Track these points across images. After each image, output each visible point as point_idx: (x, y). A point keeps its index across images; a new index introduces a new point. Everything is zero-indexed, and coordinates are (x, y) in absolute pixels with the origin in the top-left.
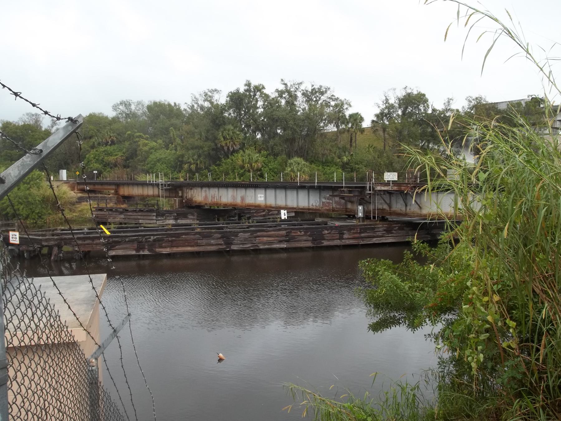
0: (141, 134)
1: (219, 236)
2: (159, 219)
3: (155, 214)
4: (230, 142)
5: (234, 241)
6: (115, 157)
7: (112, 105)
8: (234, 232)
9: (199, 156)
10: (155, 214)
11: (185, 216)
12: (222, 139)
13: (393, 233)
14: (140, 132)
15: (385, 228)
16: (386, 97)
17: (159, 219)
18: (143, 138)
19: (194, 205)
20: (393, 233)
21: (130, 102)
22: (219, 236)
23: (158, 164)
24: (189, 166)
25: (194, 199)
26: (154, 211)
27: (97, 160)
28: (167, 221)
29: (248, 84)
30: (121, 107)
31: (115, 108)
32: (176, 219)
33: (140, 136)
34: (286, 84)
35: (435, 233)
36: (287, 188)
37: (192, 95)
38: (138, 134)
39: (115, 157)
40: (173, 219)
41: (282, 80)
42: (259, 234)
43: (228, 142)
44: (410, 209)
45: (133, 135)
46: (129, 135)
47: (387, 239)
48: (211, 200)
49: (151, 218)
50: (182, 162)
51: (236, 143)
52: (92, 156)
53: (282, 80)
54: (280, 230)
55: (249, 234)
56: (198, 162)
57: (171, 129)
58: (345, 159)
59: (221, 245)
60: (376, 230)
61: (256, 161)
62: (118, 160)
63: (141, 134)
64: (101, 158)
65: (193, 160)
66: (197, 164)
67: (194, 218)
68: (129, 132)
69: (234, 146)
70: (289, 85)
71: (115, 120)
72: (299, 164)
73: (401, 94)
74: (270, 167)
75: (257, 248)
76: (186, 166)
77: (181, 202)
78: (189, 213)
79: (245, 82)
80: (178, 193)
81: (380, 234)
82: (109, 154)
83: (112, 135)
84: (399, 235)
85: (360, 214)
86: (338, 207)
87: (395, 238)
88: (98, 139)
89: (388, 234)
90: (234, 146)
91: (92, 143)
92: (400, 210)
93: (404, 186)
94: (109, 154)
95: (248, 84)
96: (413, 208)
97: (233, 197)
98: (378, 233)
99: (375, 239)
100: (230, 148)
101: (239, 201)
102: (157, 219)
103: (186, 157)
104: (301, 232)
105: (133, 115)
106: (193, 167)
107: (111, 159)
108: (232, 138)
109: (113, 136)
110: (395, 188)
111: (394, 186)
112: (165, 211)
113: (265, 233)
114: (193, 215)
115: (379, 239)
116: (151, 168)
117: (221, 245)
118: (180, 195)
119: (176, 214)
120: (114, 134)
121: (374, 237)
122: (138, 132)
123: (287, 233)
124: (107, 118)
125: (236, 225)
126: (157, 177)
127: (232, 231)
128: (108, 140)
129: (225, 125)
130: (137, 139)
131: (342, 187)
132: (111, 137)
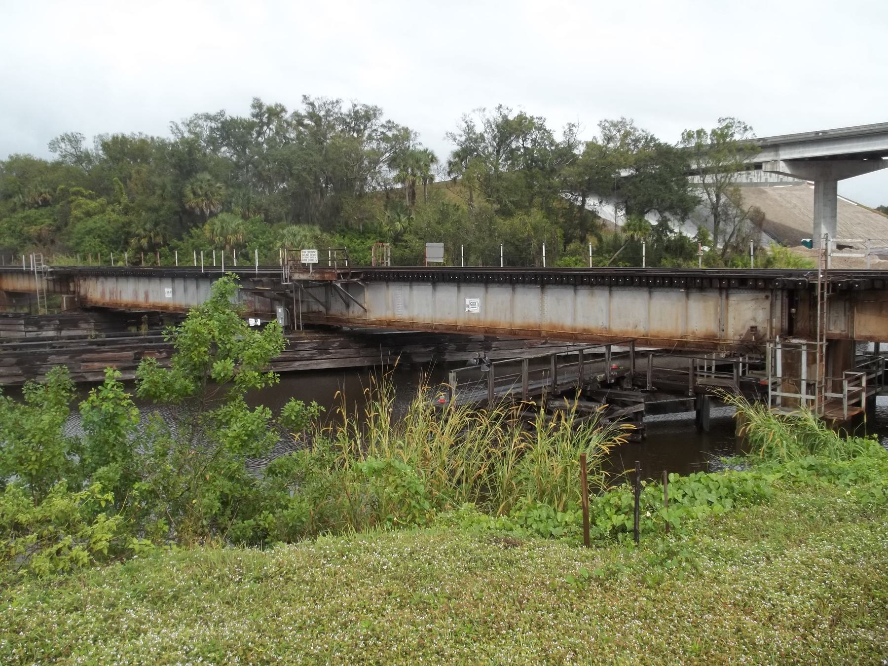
0: (81, 189)
1: (13, 360)
2: (30, 329)
3: (22, 322)
4: (203, 200)
5: (41, 369)
6: (39, 228)
7: (49, 141)
8: (40, 354)
9: (156, 224)
10: (22, 322)
11: (74, 324)
12: (192, 196)
13: (331, 353)
14: (78, 186)
15: (315, 345)
16: (466, 122)
17: (30, 329)
18: (83, 195)
19: (88, 306)
20: (331, 353)
21: (78, 136)
22: (13, 360)
23: (87, 238)
24: (139, 241)
25: (89, 296)
26: (21, 316)
27: (14, 231)
28: (44, 333)
29: (257, 105)
30: (62, 145)
31: (53, 146)
32: (59, 329)
33: (79, 191)
34: (312, 104)
35: (408, 351)
36: (549, 283)
37: (171, 124)
38: (75, 189)
39: (39, 228)
40: (54, 330)
41: (305, 97)
42: (84, 356)
43: (200, 200)
44: (353, 312)
45: (68, 191)
46: (62, 190)
47: (319, 364)
48: (110, 298)
49: (17, 327)
50: (129, 234)
51: (214, 201)
52: (6, 225)
53: (305, 97)
54: (122, 350)
55: (67, 357)
56: (152, 234)
57: (115, 181)
58: (399, 226)
59: (16, 375)
60: (298, 348)
61: (235, 232)
62: (43, 231)
63: (81, 189)
64: (18, 229)
65: (145, 230)
66: (150, 238)
67: (90, 327)
68: (62, 186)
69: (212, 206)
70: (316, 104)
71: (57, 165)
72: (295, 235)
73: (494, 116)
74: (261, 240)
75: (83, 380)
76: (133, 241)
77: (71, 301)
78: (81, 320)
79: (251, 102)
80: (69, 287)
81: (306, 354)
82: (30, 222)
83: (43, 190)
84: (342, 356)
85: (280, 321)
86: (263, 308)
87: (334, 362)
88: (23, 197)
89: (321, 354)
90: (212, 206)
91: (12, 204)
92: (341, 313)
93: (328, 273)
94: (30, 222)
95: (257, 105)
96: (355, 311)
97: (136, 294)
98: (302, 353)
99: (297, 364)
100: (205, 210)
101: (141, 299)
102: (26, 329)
103: (134, 225)
104: (160, 353)
105: (83, 158)
106: (144, 242)
107: (33, 230)
108: (206, 195)
109: (45, 193)
110: (317, 276)
111: (315, 272)
112: (41, 316)
113: (96, 356)
114: (87, 322)
115: (304, 362)
116: (78, 244)
117: (16, 375)
118: (72, 289)
119: (57, 322)
120: (47, 190)
121: (296, 360)
122: (77, 185)
123: (135, 354)
124: (46, 163)
125: (69, 341)
126: (84, 258)
127: (36, 352)
128: (36, 199)
129: (196, 172)
130: (73, 197)
131: (254, 275)
132: (42, 194)
